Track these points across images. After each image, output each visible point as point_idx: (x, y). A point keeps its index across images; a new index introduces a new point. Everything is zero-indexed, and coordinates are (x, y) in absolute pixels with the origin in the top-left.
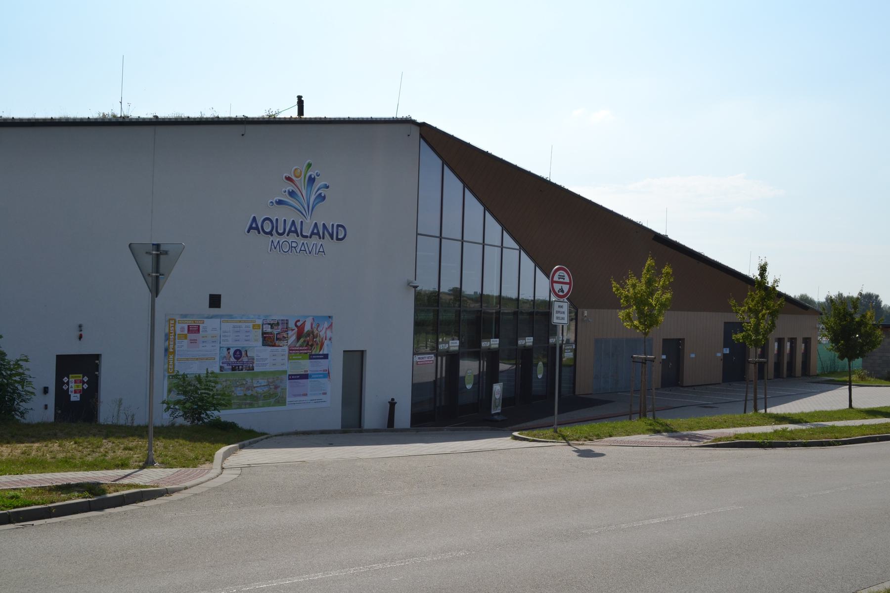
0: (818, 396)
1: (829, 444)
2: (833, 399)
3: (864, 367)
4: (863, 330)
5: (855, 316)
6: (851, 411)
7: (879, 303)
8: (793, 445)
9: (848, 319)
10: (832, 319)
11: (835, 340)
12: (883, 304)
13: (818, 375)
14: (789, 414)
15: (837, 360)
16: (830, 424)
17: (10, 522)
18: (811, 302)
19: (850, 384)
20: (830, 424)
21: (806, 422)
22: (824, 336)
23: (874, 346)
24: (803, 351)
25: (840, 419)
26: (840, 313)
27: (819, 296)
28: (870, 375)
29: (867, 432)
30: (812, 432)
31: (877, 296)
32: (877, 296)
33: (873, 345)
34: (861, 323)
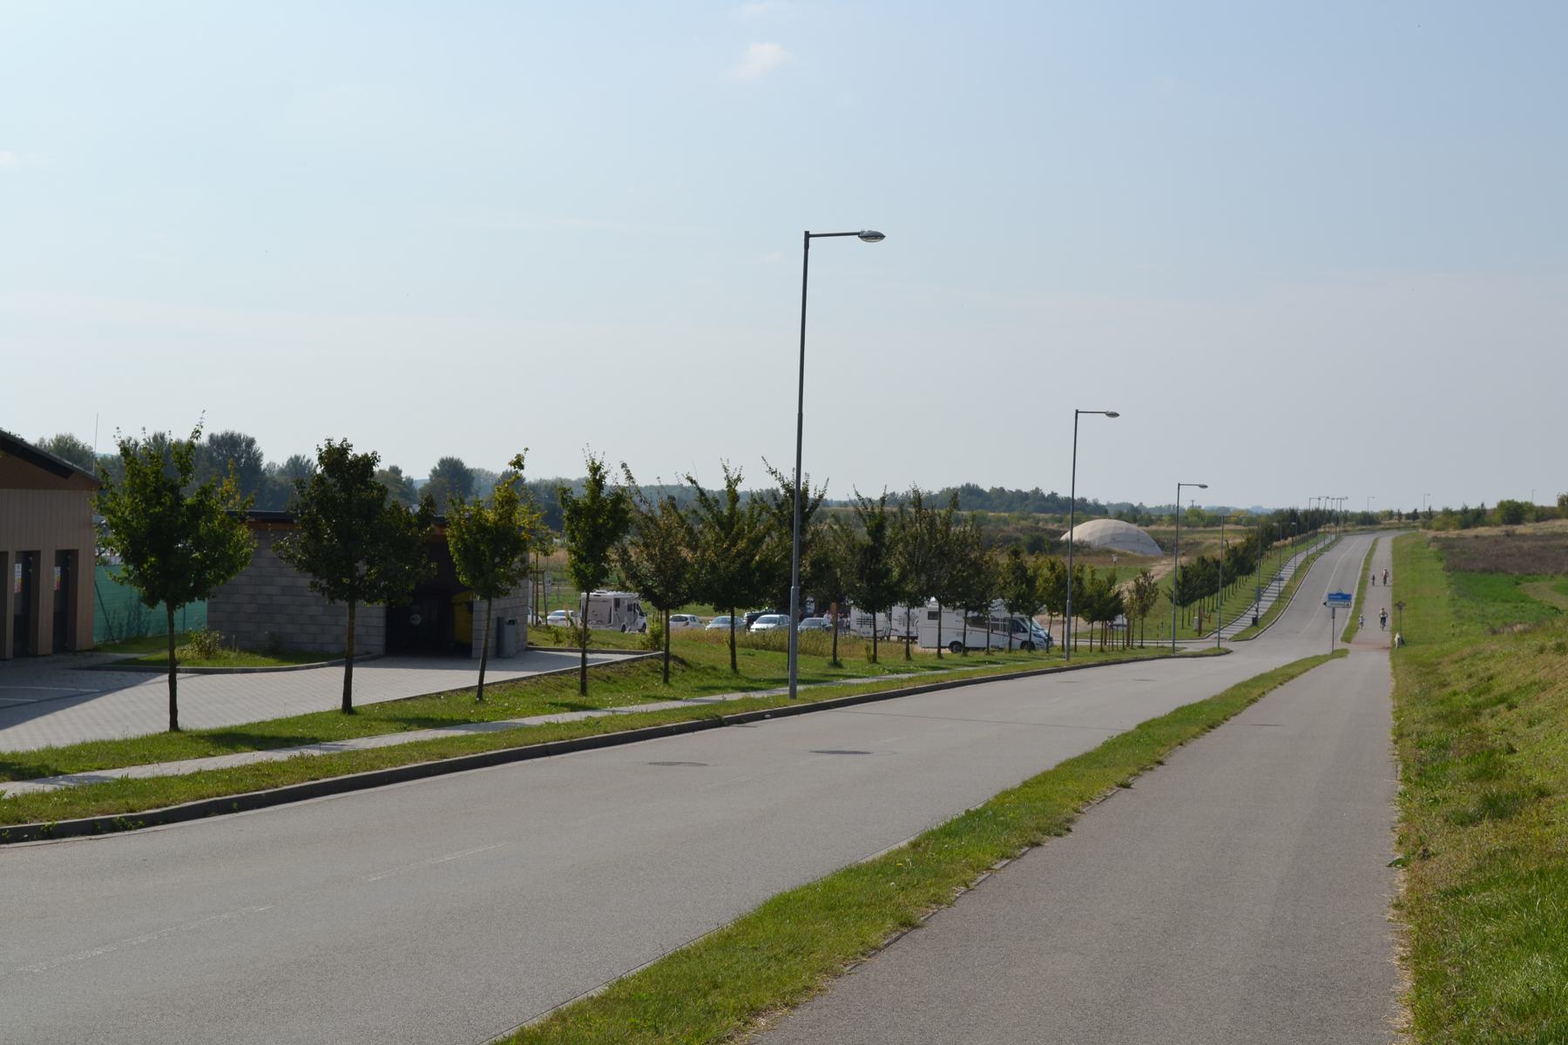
0: (95, 703)
1: (112, 827)
2: (128, 711)
3: (213, 624)
4: (203, 530)
5: (182, 491)
6: (176, 739)
7: (255, 459)
8: (761, 717)
9: (167, 499)
10: (126, 500)
11: (133, 556)
12: (265, 463)
13: (95, 649)
14: (14, 754)
15: (144, 607)
16: (117, 774)
17: (290, 801)
18: (83, 455)
19: (171, 668)
20: (117, 774)
21: (56, 773)
22: (107, 544)
23: (231, 570)
24: (56, 587)
25: (145, 760)
26: (145, 485)
27: (105, 447)
28: (226, 644)
29: (210, 788)
30: (71, 796)
31: (251, 442)
32: (251, 442)
33: (230, 565)
34: (200, 510)
